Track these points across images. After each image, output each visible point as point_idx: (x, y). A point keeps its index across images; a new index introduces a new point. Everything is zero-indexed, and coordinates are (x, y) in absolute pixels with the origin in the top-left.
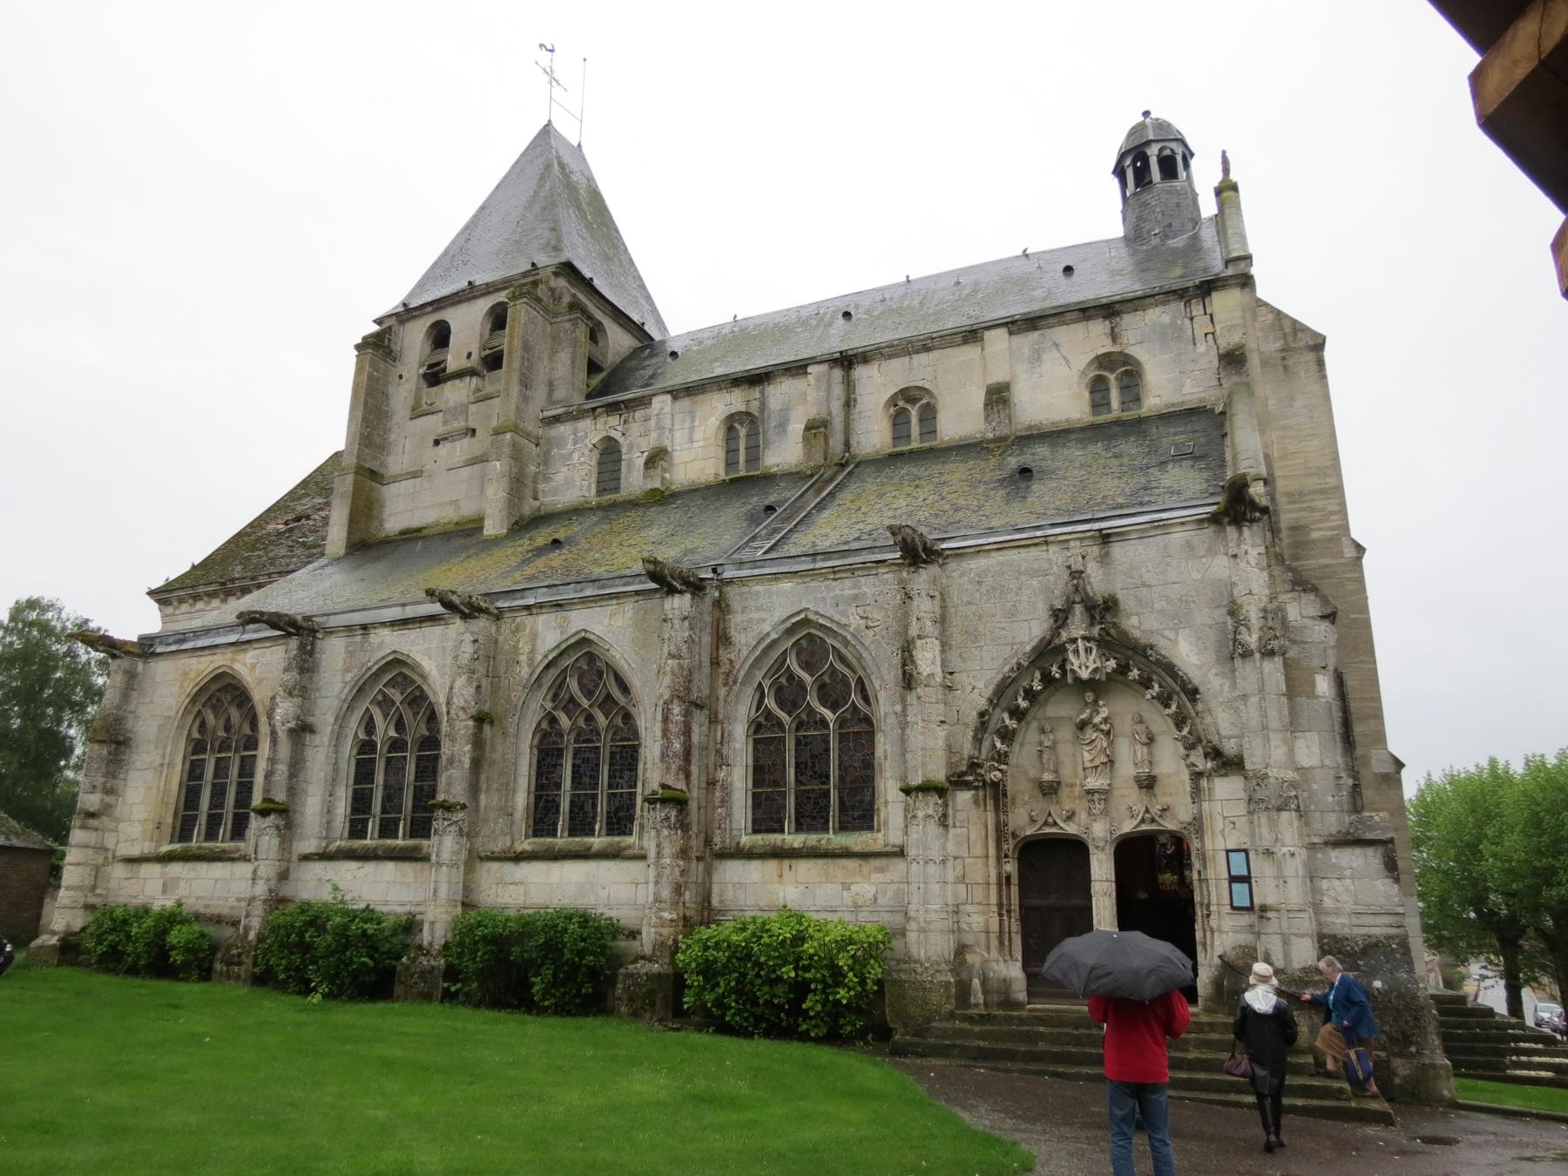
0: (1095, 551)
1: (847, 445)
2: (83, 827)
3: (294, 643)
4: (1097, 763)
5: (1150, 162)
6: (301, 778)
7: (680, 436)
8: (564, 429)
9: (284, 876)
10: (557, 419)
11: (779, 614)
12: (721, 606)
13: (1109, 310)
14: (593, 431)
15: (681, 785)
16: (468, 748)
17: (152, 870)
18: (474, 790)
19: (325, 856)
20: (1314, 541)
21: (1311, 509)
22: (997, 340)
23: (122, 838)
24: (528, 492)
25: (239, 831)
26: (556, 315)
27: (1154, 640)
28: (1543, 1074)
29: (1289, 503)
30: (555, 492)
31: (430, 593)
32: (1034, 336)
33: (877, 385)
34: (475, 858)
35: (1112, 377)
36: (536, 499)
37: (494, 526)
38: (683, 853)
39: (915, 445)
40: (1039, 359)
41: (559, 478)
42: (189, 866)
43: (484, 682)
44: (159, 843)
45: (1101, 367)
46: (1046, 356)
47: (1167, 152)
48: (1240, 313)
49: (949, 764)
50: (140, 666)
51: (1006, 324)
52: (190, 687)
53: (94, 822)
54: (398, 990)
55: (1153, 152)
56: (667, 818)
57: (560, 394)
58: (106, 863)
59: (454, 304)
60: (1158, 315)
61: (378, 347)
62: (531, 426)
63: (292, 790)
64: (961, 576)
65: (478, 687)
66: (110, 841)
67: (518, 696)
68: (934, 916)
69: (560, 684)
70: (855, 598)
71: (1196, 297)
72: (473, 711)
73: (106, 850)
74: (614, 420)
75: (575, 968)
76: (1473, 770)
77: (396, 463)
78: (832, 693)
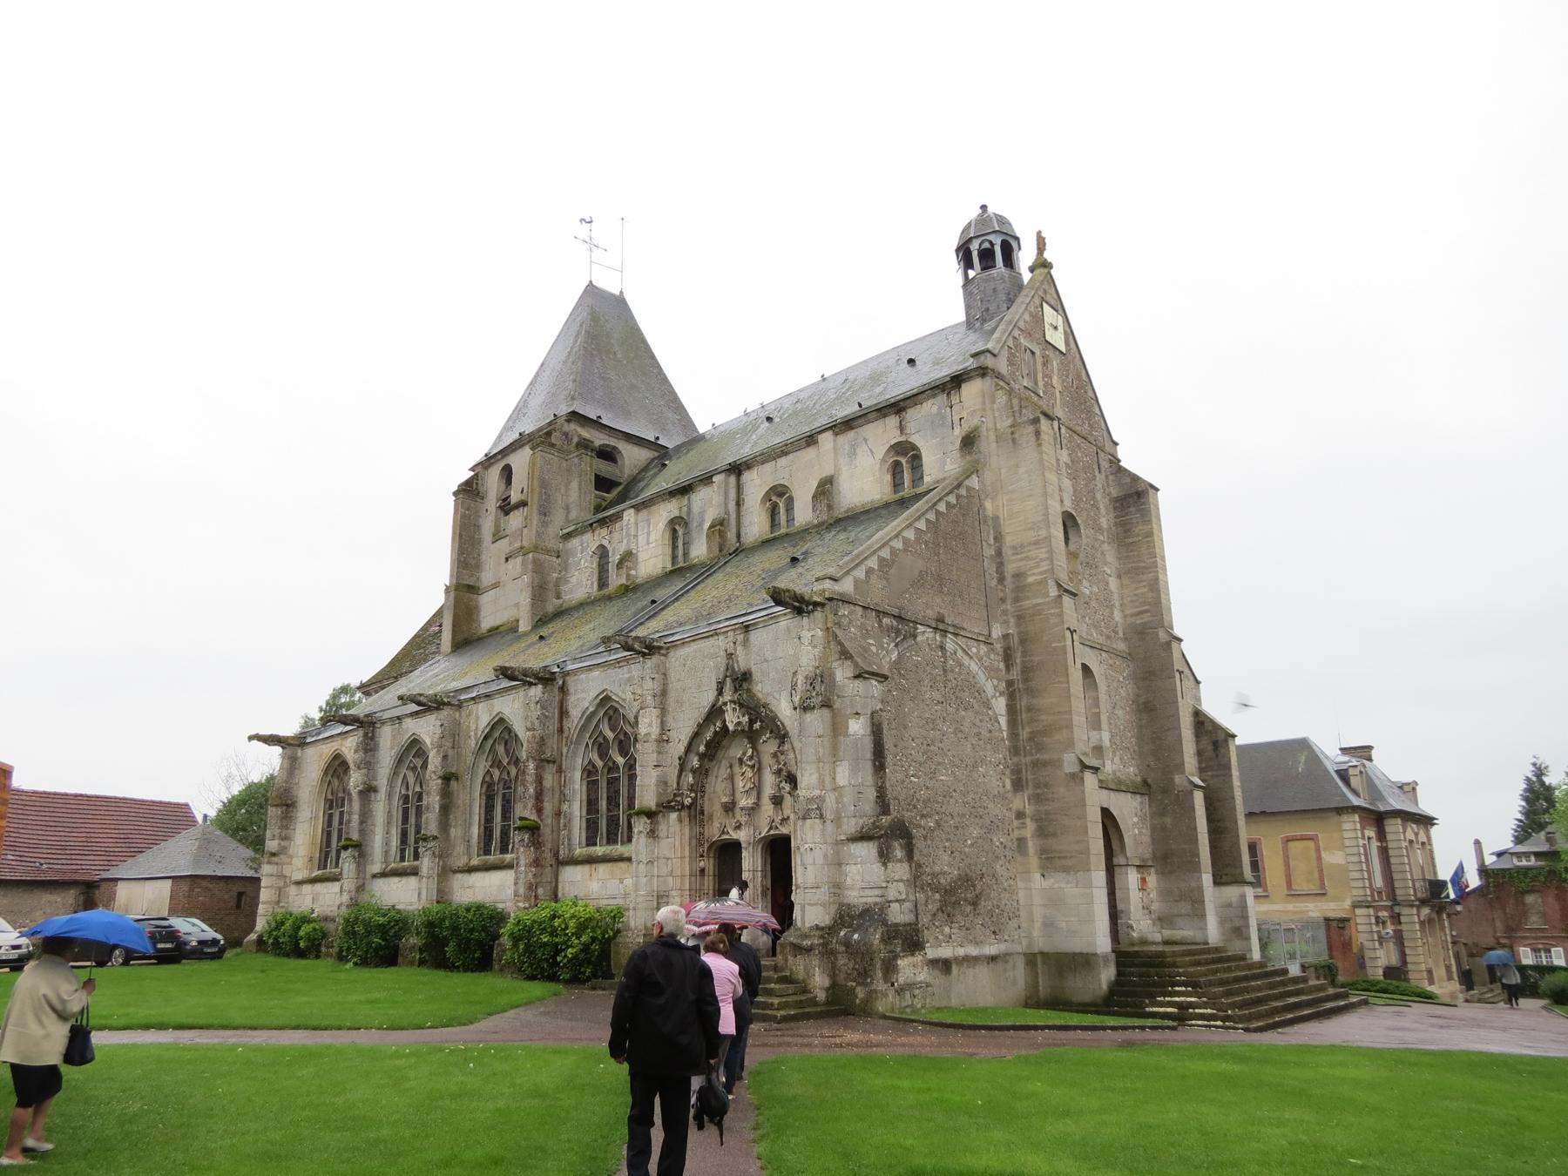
0: (741, 637)
1: (739, 536)
5: (987, 251)
7: (642, 539)
8: (575, 542)
9: (360, 888)
10: (569, 536)
11: (593, 694)
12: (563, 689)
13: (897, 408)
14: (591, 541)
15: (534, 817)
17: (307, 888)
18: (444, 825)
19: (384, 875)
20: (1030, 585)
22: (826, 439)
24: (551, 595)
26: (569, 452)
27: (770, 700)
28: (1170, 1010)
32: (851, 434)
33: (757, 483)
34: (446, 872)
35: (904, 461)
36: (558, 597)
37: (524, 627)
38: (537, 863)
39: (783, 531)
40: (855, 453)
41: (574, 580)
43: (450, 752)
44: (311, 870)
45: (898, 453)
46: (859, 451)
47: (986, 245)
48: (980, 400)
49: (659, 795)
52: (323, 765)
53: (275, 859)
54: (400, 960)
55: (974, 247)
57: (573, 515)
58: (286, 885)
60: (930, 407)
61: (469, 491)
62: (552, 543)
63: (362, 832)
64: (676, 659)
65: (445, 757)
66: (287, 872)
68: (641, 899)
70: (629, 679)
72: (440, 773)
74: (604, 531)
75: (468, 940)
76: (1330, 749)
77: (487, 578)
78: (624, 751)
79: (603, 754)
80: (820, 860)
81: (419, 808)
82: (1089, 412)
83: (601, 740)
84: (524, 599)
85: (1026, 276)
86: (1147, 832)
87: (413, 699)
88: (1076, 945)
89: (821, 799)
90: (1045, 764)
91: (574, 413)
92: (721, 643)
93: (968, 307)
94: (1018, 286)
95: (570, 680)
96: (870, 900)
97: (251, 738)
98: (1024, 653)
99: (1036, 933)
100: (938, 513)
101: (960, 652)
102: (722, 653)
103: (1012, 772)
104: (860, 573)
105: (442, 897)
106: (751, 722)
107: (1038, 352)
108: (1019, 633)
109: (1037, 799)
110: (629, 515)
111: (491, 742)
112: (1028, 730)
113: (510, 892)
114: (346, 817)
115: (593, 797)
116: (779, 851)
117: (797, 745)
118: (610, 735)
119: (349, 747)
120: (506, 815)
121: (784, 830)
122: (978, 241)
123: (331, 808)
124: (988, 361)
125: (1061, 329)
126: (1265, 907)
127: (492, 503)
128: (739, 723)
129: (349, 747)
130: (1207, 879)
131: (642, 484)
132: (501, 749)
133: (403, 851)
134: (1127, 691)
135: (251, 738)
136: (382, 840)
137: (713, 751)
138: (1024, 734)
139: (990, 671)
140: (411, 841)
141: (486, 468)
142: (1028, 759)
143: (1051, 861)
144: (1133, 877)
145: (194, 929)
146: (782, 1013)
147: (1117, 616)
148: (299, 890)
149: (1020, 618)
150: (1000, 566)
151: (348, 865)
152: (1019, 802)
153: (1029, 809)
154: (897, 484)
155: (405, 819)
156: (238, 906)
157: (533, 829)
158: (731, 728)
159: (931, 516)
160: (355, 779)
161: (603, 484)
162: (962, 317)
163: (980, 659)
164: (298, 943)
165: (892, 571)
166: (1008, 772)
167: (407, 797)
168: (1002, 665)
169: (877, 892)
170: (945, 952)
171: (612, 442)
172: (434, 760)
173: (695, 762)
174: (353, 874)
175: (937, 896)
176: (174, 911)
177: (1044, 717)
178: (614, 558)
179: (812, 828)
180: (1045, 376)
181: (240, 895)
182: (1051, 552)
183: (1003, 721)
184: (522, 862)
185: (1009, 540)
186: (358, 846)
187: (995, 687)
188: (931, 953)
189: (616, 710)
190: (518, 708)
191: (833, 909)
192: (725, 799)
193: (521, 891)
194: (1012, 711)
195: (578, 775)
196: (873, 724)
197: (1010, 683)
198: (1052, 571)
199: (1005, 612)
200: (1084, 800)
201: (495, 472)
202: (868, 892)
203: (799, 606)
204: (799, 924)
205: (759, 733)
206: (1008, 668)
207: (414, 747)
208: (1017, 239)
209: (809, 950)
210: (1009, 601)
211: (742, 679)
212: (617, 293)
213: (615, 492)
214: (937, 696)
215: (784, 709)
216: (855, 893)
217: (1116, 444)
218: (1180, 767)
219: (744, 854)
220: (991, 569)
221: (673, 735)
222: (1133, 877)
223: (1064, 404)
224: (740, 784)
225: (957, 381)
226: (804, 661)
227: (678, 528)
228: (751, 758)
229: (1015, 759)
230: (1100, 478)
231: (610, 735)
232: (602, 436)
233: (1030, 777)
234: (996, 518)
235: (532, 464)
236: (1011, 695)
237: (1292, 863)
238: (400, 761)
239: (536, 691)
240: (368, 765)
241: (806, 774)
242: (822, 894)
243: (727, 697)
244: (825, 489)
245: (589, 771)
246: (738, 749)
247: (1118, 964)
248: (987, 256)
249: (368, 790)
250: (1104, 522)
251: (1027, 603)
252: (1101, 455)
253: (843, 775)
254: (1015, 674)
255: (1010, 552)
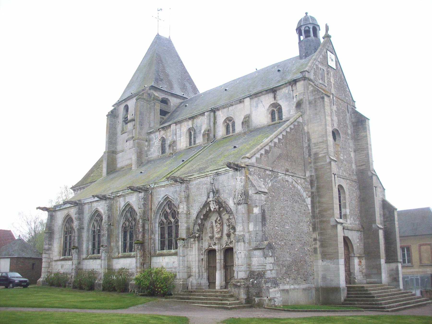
1: (214, 136)
2: (45, 253)
3: (77, 207)
4: (218, 231)
5: (308, 30)
6: (81, 240)
8: (153, 135)
9: (79, 263)
11: (162, 196)
13: (274, 91)
16: (106, 232)
17: (59, 263)
18: (109, 242)
19: (86, 259)
20: (320, 157)
21: (319, 148)
22: (247, 101)
23: (54, 255)
25: (99, 253)
29: (314, 146)
30: (151, 154)
31: (94, 196)
33: (221, 116)
34: (110, 259)
35: (275, 110)
36: (147, 156)
39: (231, 134)
41: (152, 150)
42: (65, 262)
47: (307, 28)
50: (54, 214)
51: (249, 97)
55: (303, 29)
56: (138, 248)
57: (152, 125)
58: (51, 261)
59: (129, 100)
60: (285, 91)
61: (112, 115)
67: (118, 218)
69: (126, 216)
71: (294, 84)
73: (51, 259)
78: (174, 218)
79: (166, 218)
80: (243, 256)
81: (99, 235)
82: (345, 91)
83: (165, 212)
84: (134, 158)
85: (322, 40)
86: (362, 245)
87: (97, 196)
88: (334, 284)
89: (244, 235)
90: (324, 222)
91: (152, 86)
92: (209, 179)
93: (300, 51)
94: (319, 43)
95: (154, 191)
96: (260, 270)
97: (37, 208)
98: (318, 183)
99: (320, 280)
100: (287, 132)
101: (294, 182)
102: (209, 183)
103: (313, 225)
104: (258, 155)
105: (110, 269)
106: (219, 208)
107: (325, 70)
108: (316, 175)
109: (321, 234)
110: (173, 127)
111: (125, 212)
112: (318, 210)
113: (134, 265)
114: (73, 238)
115: (163, 233)
116: (229, 252)
117: (236, 217)
118: (169, 211)
119: (73, 212)
120: (131, 237)
121: (231, 246)
122: (304, 27)
123: (66, 234)
124: (307, 75)
125: (334, 60)
126: (408, 270)
127: (121, 119)
128: (215, 208)
129: (73, 212)
130: (383, 261)
131: (177, 113)
132: (129, 215)
133: (93, 250)
134: (356, 193)
135: (37, 208)
136: (86, 246)
137: (207, 216)
138: (317, 211)
139: (305, 188)
140: (96, 247)
141: (118, 106)
142: (318, 220)
143: (325, 256)
144: (356, 261)
145: (16, 276)
146: (231, 306)
147: (354, 166)
148: (58, 264)
149: (316, 170)
150: (309, 151)
151: (75, 255)
152: (315, 235)
153: (318, 238)
154: (273, 119)
155: (94, 239)
156: (33, 268)
157: (142, 244)
158: (212, 210)
159: (284, 133)
160: (75, 224)
161: (163, 113)
162: (298, 54)
163: (302, 185)
164: (58, 282)
165: (269, 154)
166: (311, 225)
167: (94, 231)
168: (309, 186)
169: (262, 267)
170: (287, 287)
171: (166, 97)
172: (105, 218)
173: (200, 222)
174: (76, 258)
175: (285, 268)
176: (11, 270)
177: (324, 205)
178: (168, 142)
179: (240, 245)
180: (328, 78)
181: (33, 264)
182: (327, 146)
183: (310, 207)
184: (138, 255)
185: (313, 141)
186: (77, 248)
187: (307, 195)
188: (282, 287)
189: (171, 202)
190: (134, 200)
191: (248, 272)
192: (210, 235)
193: (138, 265)
194: (313, 202)
195: (157, 225)
196: (262, 210)
197: (312, 193)
198: (327, 153)
199: (311, 167)
200: (337, 234)
201: (122, 107)
202: (260, 267)
203: (236, 168)
204: (236, 278)
205: (222, 212)
206: (312, 187)
207: (97, 214)
208: (318, 26)
209: (239, 286)
210: (312, 163)
211: (216, 192)
212: (168, 37)
213: (167, 116)
214: (285, 198)
215: (231, 204)
216: (255, 267)
217: (355, 102)
218: (375, 222)
219: (217, 254)
220: (306, 151)
221: (192, 211)
222: (356, 261)
223: (335, 88)
224: (215, 229)
225: (295, 82)
226: (238, 187)
227: (192, 133)
228: (219, 220)
229: (314, 220)
230: (348, 115)
231: (169, 211)
232: (162, 94)
233: (319, 226)
234: (308, 133)
235: (136, 106)
236: (313, 197)
237: (422, 254)
238: (91, 219)
239: (142, 195)
240: (80, 219)
241: (239, 227)
242: (243, 268)
243: (211, 199)
244: (246, 121)
245: (161, 224)
246: (214, 218)
247: (348, 291)
248: (307, 32)
249: (81, 229)
250: (349, 132)
251: (319, 164)
252: (349, 106)
253: (251, 227)
254: (314, 190)
255: (313, 145)
